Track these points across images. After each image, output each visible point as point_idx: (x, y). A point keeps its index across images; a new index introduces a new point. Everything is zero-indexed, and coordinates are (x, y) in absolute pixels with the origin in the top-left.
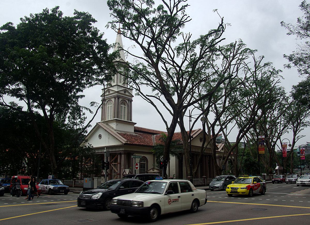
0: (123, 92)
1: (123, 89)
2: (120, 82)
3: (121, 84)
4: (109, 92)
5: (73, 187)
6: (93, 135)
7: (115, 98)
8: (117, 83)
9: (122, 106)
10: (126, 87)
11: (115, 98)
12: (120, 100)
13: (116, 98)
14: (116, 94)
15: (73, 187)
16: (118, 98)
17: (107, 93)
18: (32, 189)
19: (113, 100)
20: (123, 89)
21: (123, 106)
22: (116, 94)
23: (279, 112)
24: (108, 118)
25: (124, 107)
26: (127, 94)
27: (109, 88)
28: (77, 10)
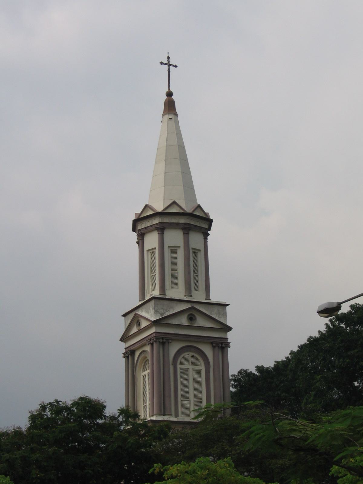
0: (184, 320)
2: (174, 285)
3: (178, 293)
7: (152, 344)
9: (187, 367)
11: (152, 344)
14: (153, 330)
17: (135, 330)
19: (148, 348)
21: (191, 367)
22: (153, 330)
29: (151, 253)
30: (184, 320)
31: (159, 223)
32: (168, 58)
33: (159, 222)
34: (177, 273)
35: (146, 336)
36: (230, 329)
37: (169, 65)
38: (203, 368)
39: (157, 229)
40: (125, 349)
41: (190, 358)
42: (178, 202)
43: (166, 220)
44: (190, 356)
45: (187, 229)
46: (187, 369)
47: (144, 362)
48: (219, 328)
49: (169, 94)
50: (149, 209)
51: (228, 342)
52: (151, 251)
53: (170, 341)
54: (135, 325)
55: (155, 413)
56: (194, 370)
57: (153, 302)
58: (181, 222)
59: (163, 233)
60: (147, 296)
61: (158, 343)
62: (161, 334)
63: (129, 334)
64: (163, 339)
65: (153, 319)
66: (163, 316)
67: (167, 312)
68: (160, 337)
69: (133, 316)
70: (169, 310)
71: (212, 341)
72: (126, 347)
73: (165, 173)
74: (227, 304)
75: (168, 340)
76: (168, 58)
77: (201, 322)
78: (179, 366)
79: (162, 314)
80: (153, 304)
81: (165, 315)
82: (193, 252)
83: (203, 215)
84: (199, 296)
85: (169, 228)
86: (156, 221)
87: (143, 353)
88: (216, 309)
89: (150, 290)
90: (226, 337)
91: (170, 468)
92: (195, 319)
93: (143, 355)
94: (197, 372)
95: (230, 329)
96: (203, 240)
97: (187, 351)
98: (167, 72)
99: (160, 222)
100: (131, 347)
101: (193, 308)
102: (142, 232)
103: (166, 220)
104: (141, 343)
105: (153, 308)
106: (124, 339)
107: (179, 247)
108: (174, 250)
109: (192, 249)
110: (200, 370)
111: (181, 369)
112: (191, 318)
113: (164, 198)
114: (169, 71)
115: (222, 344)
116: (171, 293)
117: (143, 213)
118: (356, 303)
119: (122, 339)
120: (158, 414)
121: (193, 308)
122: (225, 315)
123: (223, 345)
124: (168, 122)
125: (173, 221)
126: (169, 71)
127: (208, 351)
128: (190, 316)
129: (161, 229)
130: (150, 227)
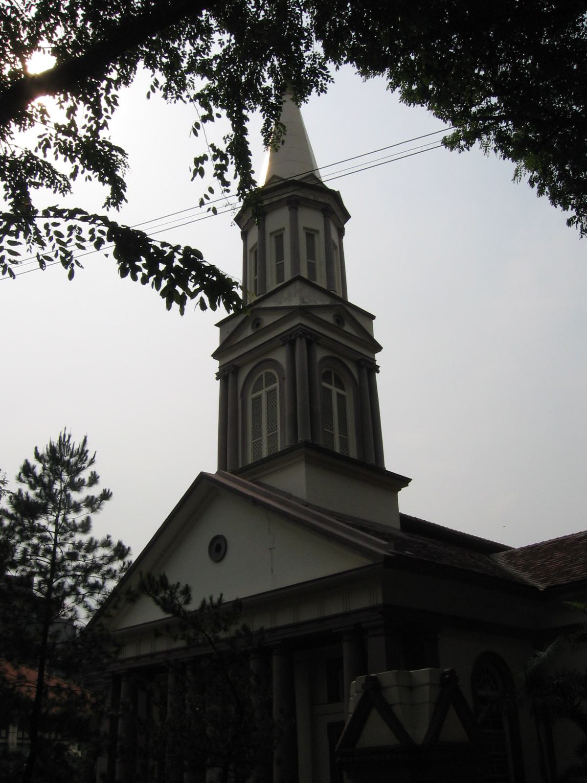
0: (329, 318)
1: (327, 301)
4: (258, 325)
7: (292, 344)
16: (310, 344)
17: (249, 332)
21: (335, 390)
25: (338, 394)
26: (348, 328)
29: (276, 237)
30: (329, 318)
56: (338, 394)
107: (283, 229)
108: (311, 235)
109: (305, 228)
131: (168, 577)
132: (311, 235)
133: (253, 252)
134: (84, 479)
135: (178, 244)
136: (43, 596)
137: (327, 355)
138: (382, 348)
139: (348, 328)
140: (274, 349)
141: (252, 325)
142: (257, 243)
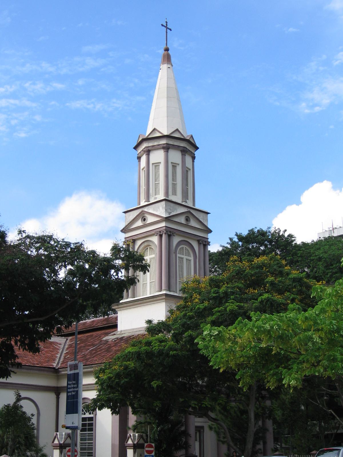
0: (182, 220)
1: (182, 210)
2: (174, 193)
3: (178, 198)
4: (144, 220)
5: (68, 401)
6: (130, 225)
7: (161, 236)
8: (167, 193)
9: (182, 256)
10: (191, 206)
11: (161, 236)
12: (176, 240)
13: (164, 236)
14: (163, 224)
15: (68, 401)
16: (169, 236)
17: (139, 223)
18: (258, 257)
19: (155, 239)
20: (182, 210)
21: (185, 257)
22: (163, 224)
23: (236, 409)
24: (144, 291)
25: (187, 260)
26: (193, 223)
27: (146, 209)
28: (74, 243)
29: (156, 166)
30: (182, 220)
31: (166, 143)
32: (167, 22)
33: (166, 143)
34: (176, 184)
35: (173, 227)
36: (210, 231)
37: (166, 27)
38: (192, 258)
39: (163, 148)
40: (125, 238)
41: (184, 249)
42: (179, 130)
43: (171, 142)
44: (184, 248)
45: (184, 151)
46: (182, 258)
47: (145, 249)
48: (202, 229)
49: (167, 50)
50: (156, 131)
51: (209, 241)
52: (155, 165)
53: (175, 235)
54: (139, 219)
55: (163, 289)
56: (187, 260)
57: (164, 202)
58: (181, 146)
59: (168, 152)
60: (151, 198)
61: (167, 235)
62: (170, 229)
63: (130, 228)
64: (170, 232)
65: (164, 215)
66: (170, 214)
67: (173, 212)
68: (168, 230)
69: (141, 211)
70: (174, 211)
71: (199, 239)
72: (126, 237)
73: (167, 107)
74: (208, 212)
75: (173, 233)
76: (167, 22)
77: (193, 223)
78: (178, 255)
79: (170, 213)
80: (164, 205)
81: (171, 215)
82: (173, 166)
83: (193, 142)
84: (190, 204)
85: (172, 148)
86: (163, 142)
87: (146, 242)
88: (202, 214)
89: (154, 194)
90: (207, 237)
91: (32, 422)
92: (190, 221)
93: (146, 244)
94: (188, 261)
95: (210, 231)
96: (191, 160)
97: (183, 244)
98: (166, 33)
99: (167, 143)
100: (134, 237)
101: (189, 212)
102: (149, 149)
103: (171, 142)
104: (147, 234)
105: (163, 208)
106: (124, 231)
107: (160, 163)
108: (174, 166)
109: (172, 163)
110: (190, 260)
111: (179, 258)
112: (187, 219)
113: (167, 126)
114: (167, 33)
115: (205, 242)
116: (172, 198)
117: (151, 134)
118: (249, 231)
119: (124, 230)
120: (167, 290)
121: (189, 212)
122: (207, 220)
123: (206, 243)
124: (167, 70)
125: (175, 144)
126: (167, 33)
127: (195, 245)
128: (187, 218)
129: (167, 148)
130: (157, 146)
131: (148, 219)
132: (174, 166)
133: (143, 170)
134: (99, 410)
135: (93, 249)
136: (311, 453)
137: (180, 240)
138: (212, 231)
139: (193, 223)
140: (153, 235)
141: (142, 220)
142: (144, 167)
